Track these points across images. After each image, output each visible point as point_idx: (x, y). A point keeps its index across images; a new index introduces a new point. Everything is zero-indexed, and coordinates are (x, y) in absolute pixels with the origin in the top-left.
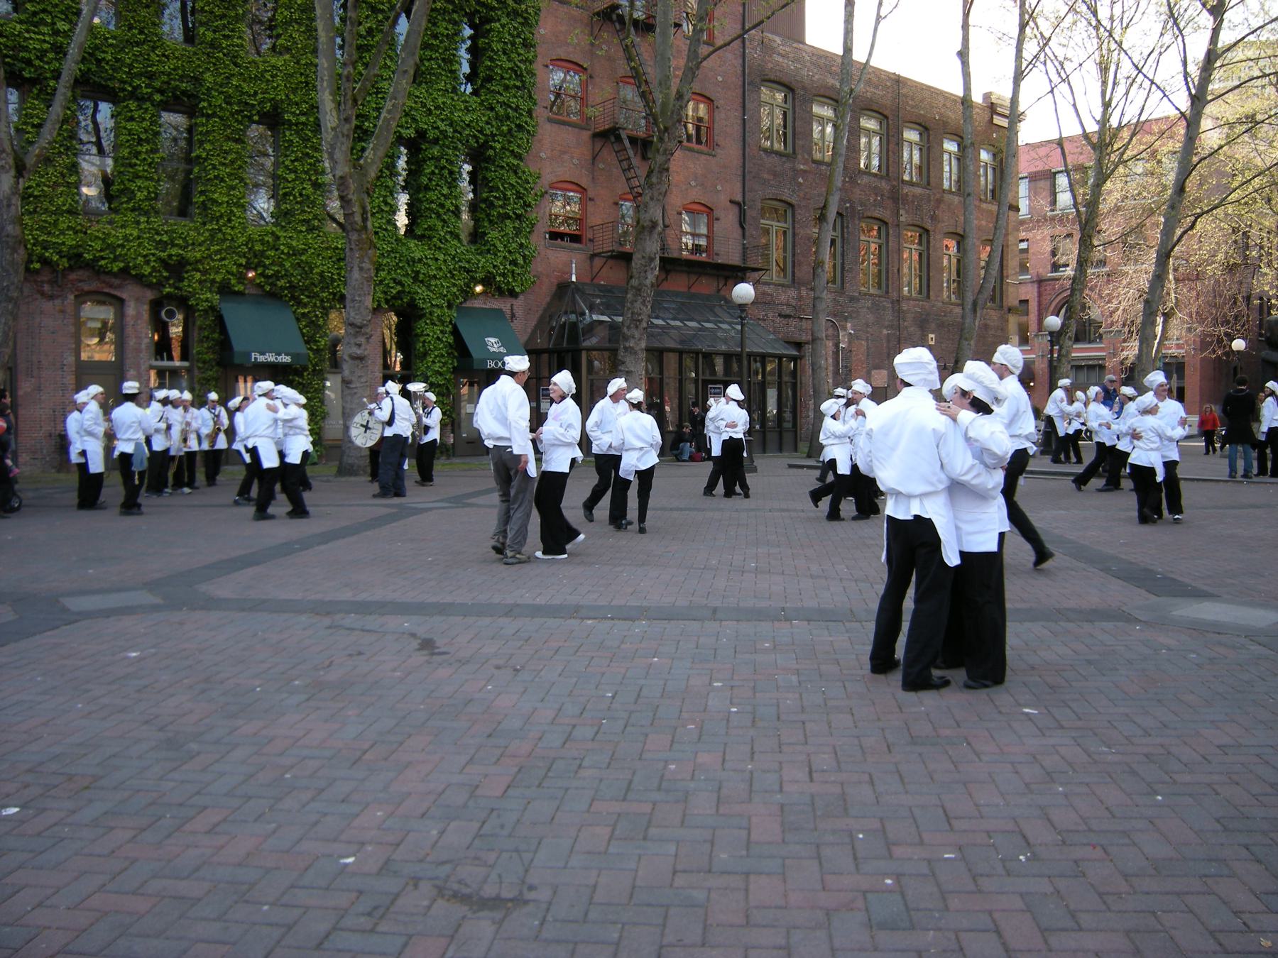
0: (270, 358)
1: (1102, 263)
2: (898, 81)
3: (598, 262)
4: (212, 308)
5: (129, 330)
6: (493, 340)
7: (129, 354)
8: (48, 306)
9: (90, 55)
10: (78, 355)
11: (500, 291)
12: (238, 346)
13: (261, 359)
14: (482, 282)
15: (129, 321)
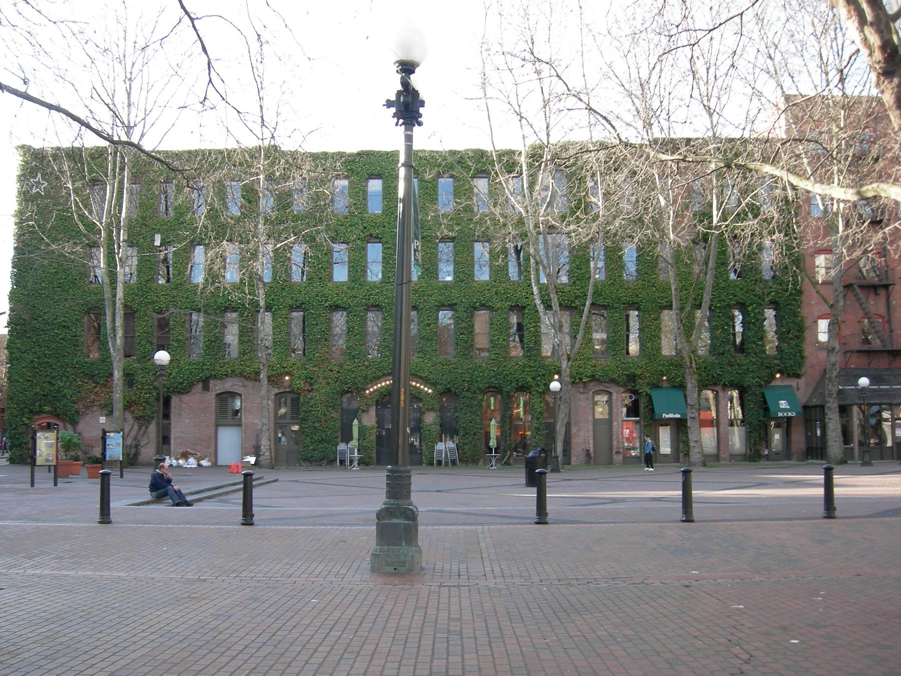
0: (671, 416)
1: (883, 82)
2: (453, 153)
3: (848, 355)
4: (647, 394)
5: (614, 405)
6: (783, 402)
7: (614, 415)
8: (582, 396)
9: (596, 293)
10: (594, 415)
11: (789, 376)
12: (657, 411)
13: (667, 416)
14: (779, 372)
15: (614, 401)
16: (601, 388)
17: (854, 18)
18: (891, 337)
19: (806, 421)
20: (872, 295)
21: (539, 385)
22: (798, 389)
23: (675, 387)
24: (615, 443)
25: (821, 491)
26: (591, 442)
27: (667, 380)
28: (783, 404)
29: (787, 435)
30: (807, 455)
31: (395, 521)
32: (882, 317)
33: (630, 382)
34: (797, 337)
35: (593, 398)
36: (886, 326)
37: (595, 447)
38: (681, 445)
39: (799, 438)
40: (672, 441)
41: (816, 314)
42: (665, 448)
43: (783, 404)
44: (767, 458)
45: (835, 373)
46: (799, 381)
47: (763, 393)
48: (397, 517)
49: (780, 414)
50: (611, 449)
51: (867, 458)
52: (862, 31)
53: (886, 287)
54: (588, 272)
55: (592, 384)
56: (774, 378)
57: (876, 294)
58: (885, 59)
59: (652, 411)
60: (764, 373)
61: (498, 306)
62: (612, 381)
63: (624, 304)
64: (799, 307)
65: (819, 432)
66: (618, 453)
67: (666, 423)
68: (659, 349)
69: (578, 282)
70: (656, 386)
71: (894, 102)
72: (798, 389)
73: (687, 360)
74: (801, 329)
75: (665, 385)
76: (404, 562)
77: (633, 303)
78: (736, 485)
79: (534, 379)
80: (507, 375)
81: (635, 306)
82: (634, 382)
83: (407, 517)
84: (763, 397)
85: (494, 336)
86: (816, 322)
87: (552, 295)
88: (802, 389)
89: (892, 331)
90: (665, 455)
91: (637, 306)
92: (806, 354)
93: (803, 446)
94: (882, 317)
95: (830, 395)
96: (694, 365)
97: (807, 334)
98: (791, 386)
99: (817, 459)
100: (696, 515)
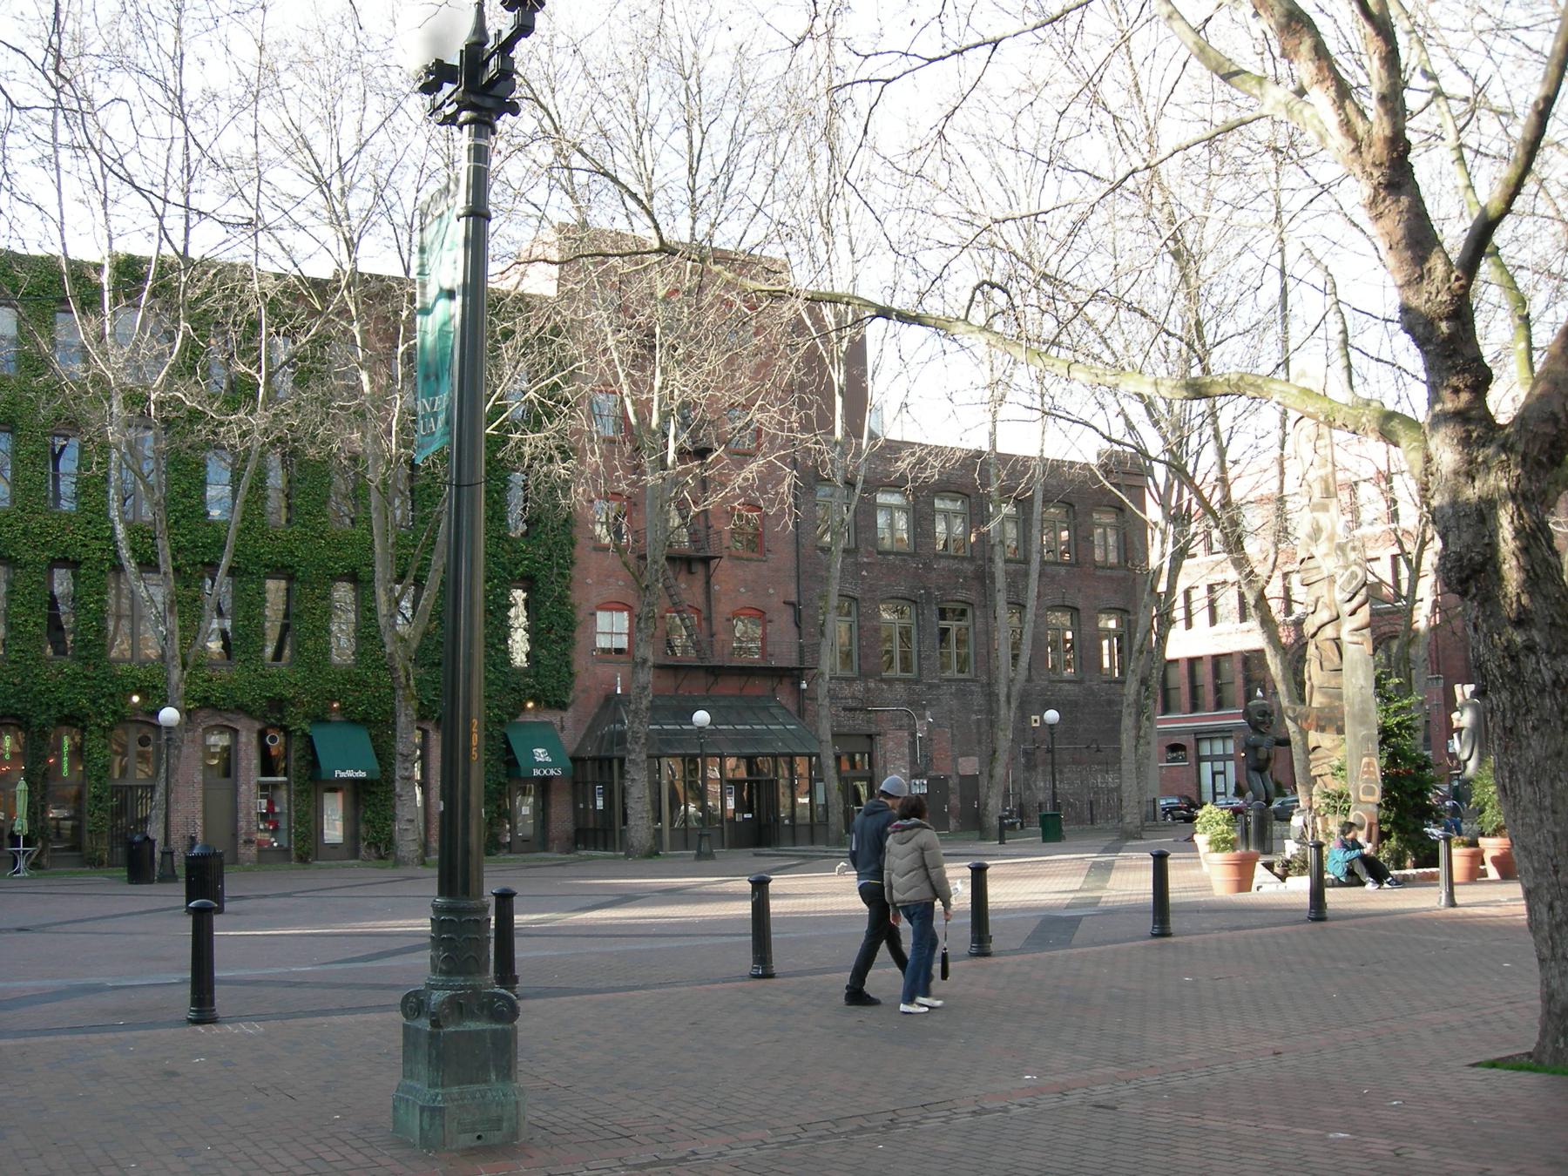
0: (350, 774)
4: (305, 735)
11: (549, 706)
13: (343, 775)
14: (532, 698)
16: (219, 721)
17: (1328, 83)
18: (711, 644)
19: (575, 783)
20: (683, 576)
21: (102, 714)
22: (562, 728)
23: (353, 721)
24: (242, 824)
25: (745, 909)
26: (199, 822)
27: (340, 709)
28: (540, 754)
29: (542, 812)
30: (576, 843)
31: (472, 1026)
32: (698, 611)
33: (273, 711)
34: (564, 639)
35: (204, 740)
36: (704, 624)
37: (205, 832)
38: (363, 829)
39: (562, 817)
40: (345, 820)
41: (596, 600)
42: (334, 830)
43: (540, 754)
44: (510, 848)
45: (645, 703)
46: (563, 714)
47: (505, 735)
48: (473, 1016)
49: (536, 772)
50: (235, 835)
51: (705, 847)
52: (1341, 107)
53: (706, 561)
54: (203, 503)
55: (202, 714)
56: (523, 708)
57: (690, 572)
58: (1392, 160)
59: (314, 764)
60: (508, 700)
61: (28, 557)
62: (242, 709)
63: (266, 566)
64: (568, 588)
65: (600, 803)
66: (249, 842)
67: (334, 786)
68: (326, 652)
69: (183, 522)
70: (319, 719)
71: (1404, 237)
72: (562, 728)
73: (402, 673)
74: (570, 626)
75: (335, 717)
76: (500, 1120)
77: (284, 567)
78: (1359, 921)
79: (94, 702)
80: (40, 692)
81: (279, 571)
82: (281, 711)
83: (496, 1016)
84: (507, 742)
85: (16, 615)
86: (594, 614)
87: (159, 542)
88: (570, 727)
89: (712, 636)
90: (334, 846)
91: (290, 571)
92: (576, 668)
93: (569, 827)
94: (698, 611)
95: (636, 740)
96: (412, 682)
97: (579, 635)
98: (551, 723)
99: (596, 849)
100: (777, 965)
